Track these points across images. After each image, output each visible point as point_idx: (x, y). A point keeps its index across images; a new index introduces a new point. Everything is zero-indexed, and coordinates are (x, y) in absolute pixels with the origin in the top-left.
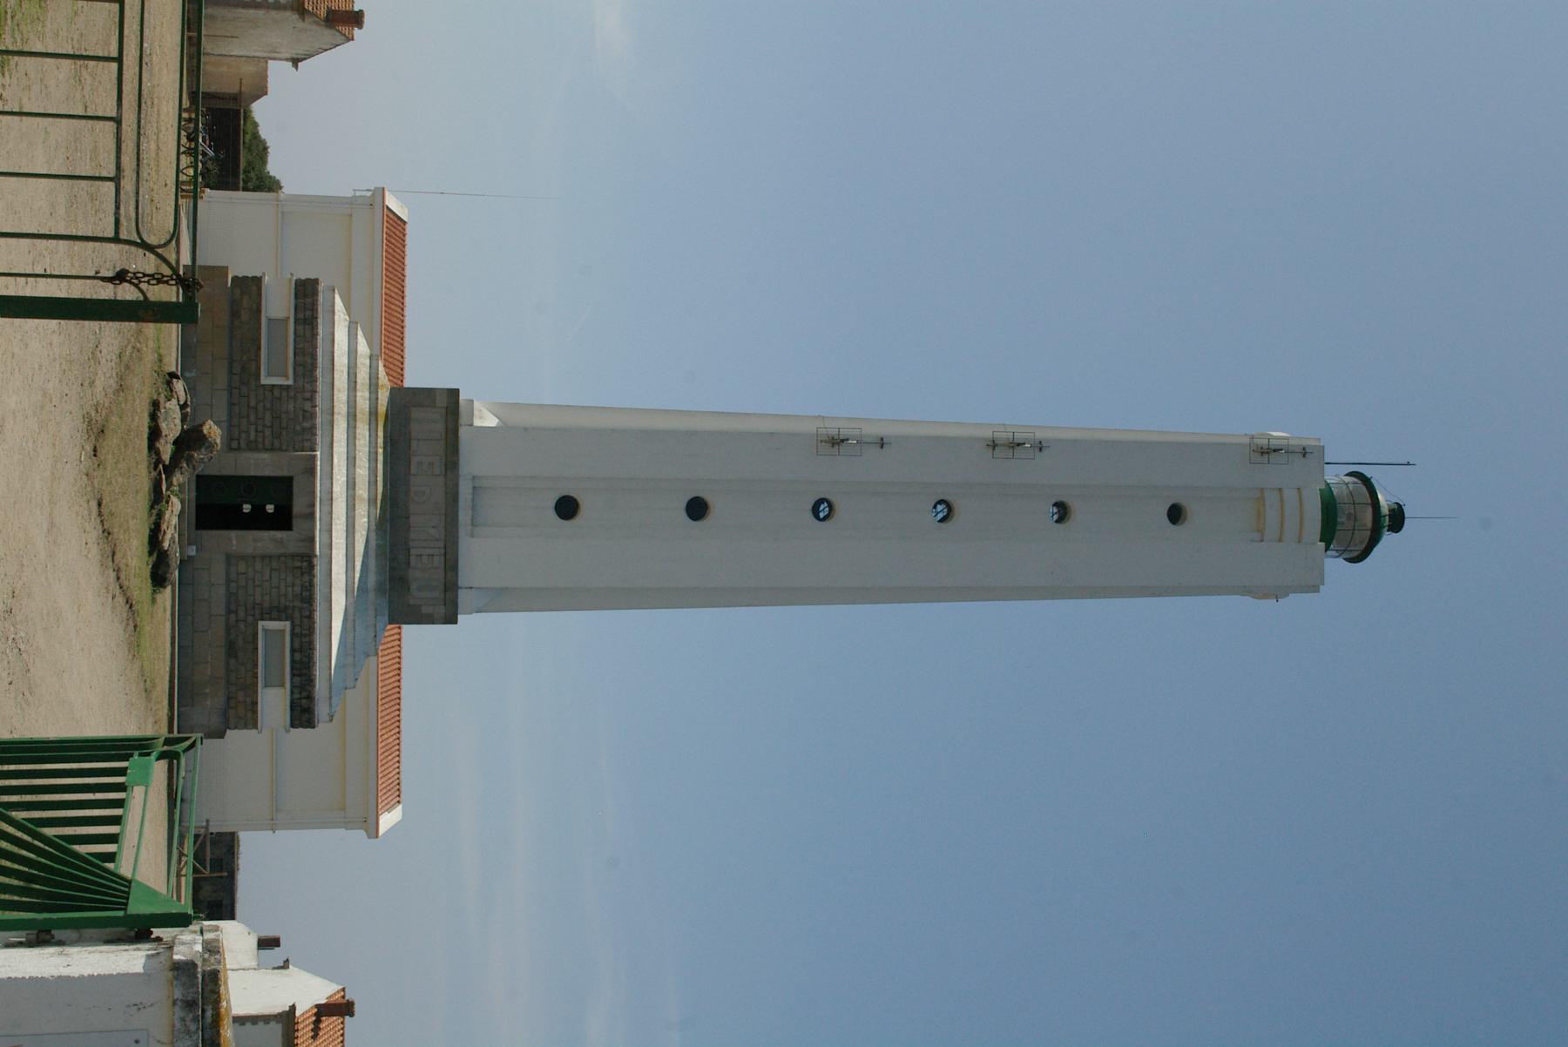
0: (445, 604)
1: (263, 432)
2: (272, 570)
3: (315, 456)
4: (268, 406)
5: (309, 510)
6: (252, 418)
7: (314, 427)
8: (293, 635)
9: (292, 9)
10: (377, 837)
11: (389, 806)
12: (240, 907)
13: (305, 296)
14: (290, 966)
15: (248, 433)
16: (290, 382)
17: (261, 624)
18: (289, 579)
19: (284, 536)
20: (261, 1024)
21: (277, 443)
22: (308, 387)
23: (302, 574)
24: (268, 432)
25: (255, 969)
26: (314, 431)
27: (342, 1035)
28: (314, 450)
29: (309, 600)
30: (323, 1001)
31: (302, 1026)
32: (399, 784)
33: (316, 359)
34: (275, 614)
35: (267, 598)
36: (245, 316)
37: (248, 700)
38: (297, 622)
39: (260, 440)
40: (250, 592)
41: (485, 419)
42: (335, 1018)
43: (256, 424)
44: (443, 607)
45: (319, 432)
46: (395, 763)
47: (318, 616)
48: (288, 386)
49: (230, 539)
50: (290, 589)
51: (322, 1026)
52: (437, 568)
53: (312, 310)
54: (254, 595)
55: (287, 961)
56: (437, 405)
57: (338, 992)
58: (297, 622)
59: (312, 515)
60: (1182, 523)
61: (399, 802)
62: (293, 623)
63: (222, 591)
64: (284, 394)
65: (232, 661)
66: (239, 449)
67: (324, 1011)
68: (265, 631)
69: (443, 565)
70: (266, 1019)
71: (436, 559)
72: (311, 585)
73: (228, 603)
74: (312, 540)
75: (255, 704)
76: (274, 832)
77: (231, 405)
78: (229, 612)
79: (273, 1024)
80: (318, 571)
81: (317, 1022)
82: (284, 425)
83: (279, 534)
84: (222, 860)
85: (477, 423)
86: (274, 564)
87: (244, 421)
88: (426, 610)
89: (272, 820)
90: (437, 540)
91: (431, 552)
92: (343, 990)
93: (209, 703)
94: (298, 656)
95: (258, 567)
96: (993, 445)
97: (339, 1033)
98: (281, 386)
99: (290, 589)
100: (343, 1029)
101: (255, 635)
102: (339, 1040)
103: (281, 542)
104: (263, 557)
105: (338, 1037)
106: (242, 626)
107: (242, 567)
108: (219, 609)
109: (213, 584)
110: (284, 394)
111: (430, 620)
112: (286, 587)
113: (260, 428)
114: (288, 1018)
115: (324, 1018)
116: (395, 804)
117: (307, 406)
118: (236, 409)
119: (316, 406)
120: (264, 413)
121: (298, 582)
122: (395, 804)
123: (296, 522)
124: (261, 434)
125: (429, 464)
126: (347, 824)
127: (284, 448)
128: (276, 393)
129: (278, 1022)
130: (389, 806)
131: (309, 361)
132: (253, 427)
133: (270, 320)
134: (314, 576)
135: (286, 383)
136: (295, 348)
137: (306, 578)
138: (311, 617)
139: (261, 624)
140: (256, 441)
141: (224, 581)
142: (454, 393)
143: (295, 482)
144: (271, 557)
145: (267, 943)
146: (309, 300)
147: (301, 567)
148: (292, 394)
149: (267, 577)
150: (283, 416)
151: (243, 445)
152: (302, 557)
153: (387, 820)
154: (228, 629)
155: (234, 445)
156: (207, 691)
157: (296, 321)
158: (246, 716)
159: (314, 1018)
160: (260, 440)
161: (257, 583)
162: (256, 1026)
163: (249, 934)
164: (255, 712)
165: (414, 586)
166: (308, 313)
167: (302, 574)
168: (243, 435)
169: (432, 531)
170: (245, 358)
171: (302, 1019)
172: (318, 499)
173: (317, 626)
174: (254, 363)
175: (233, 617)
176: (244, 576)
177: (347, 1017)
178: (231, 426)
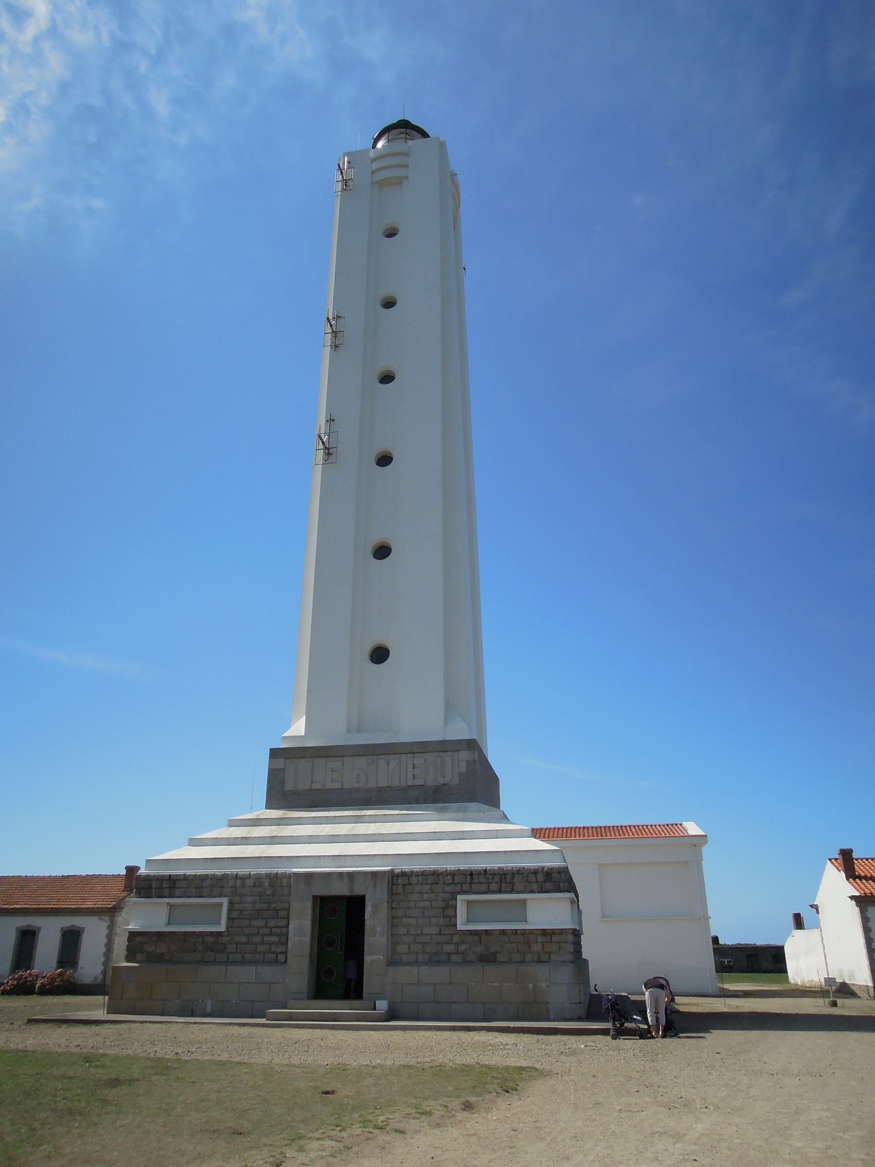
0: (458, 751)
1: (271, 928)
2: (406, 916)
4: (246, 922)
5: (346, 880)
6: (257, 939)
7: (268, 875)
9: (113, 916)
10: (706, 836)
11: (683, 830)
12: (774, 942)
13: (150, 888)
14: (815, 903)
15: (271, 944)
16: (225, 901)
17: (460, 927)
18: (415, 897)
19: (370, 904)
20: (870, 925)
21: (283, 913)
22: (231, 883)
23: (410, 884)
24: (272, 923)
26: (272, 875)
27: (867, 859)
30: (843, 874)
31: (866, 890)
32: (668, 825)
34: (450, 912)
36: (162, 949)
37: (540, 939)
38: (458, 888)
39: (278, 931)
40: (428, 938)
41: (298, 728)
42: (856, 867)
43: (263, 935)
44: (460, 752)
45: (275, 870)
46: (656, 828)
47: (451, 867)
49: (372, 962)
50: (426, 896)
51: (862, 874)
52: (425, 760)
53: (163, 880)
54: (431, 935)
56: (283, 767)
57: (833, 863)
58: (458, 888)
59: (351, 875)
61: (681, 825)
62: (459, 893)
63: (425, 970)
65: (500, 958)
66: (285, 953)
67: (851, 874)
68: (469, 921)
69: (422, 755)
70: (865, 921)
71: (416, 761)
72: (423, 874)
73: (438, 962)
74: (374, 874)
75: (544, 932)
76: (710, 917)
77: (243, 962)
78: (448, 961)
79: (868, 914)
80: (406, 868)
81: (860, 877)
83: (368, 910)
84: (747, 955)
87: (260, 948)
89: (701, 919)
90: (400, 761)
91: (410, 767)
92: (830, 860)
93: (544, 985)
94: (494, 886)
95: (402, 931)
96: (335, 347)
97: (866, 862)
98: (229, 910)
100: (862, 859)
101: (471, 933)
102: (872, 862)
103: (375, 907)
105: (870, 863)
106: (463, 947)
107: (403, 948)
108: (441, 973)
109: (418, 981)
110: (237, 906)
112: (423, 900)
113: (267, 931)
114: (862, 901)
115: (857, 873)
116: (682, 827)
117: (250, 882)
118: (248, 956)
119: (237, 875)
120: (253, 927)
121: (418, 888)
122: (682, 827)
123: (358, 891)
124: (273, 930)
126: (699, 859)
127: (287, 905)
128: (235, 915)
130: (683, 830)
131: (208, 882)
132: (266, 939)
133: (169, 923)
134: (412, 872)
136: (195, 897)
137: (414, 880)
138: (454, 874)
139: (460, 927)
140: (280, 935)
141: (415, 968)
142: (275, 753)
145: (798, 922)
148: (237, 899)
149: (413, 921)
150: (257, 907)
151: (283, 949)
152: (393, 884)
153: (693, 829)
154: (466, 962)
155: (281, 958)
156: (531, 986)
157: (171, 896)
158: (557, 943)
159: (864, 881)
160: (278, 931)
161: (420, 932)
162: (872, 928)
163: (793, 936)
164: (553, 932)
167: (410, 884)
168: (273, 948)
169: (391, 767)
170: (201, 948)
171: (861, 890)
172: (337, 869)
173: (462, 867)
174: (207, 939)
175: (454, 958)
176: (411, 946)
177: (854, 855)
178: (264, 962)
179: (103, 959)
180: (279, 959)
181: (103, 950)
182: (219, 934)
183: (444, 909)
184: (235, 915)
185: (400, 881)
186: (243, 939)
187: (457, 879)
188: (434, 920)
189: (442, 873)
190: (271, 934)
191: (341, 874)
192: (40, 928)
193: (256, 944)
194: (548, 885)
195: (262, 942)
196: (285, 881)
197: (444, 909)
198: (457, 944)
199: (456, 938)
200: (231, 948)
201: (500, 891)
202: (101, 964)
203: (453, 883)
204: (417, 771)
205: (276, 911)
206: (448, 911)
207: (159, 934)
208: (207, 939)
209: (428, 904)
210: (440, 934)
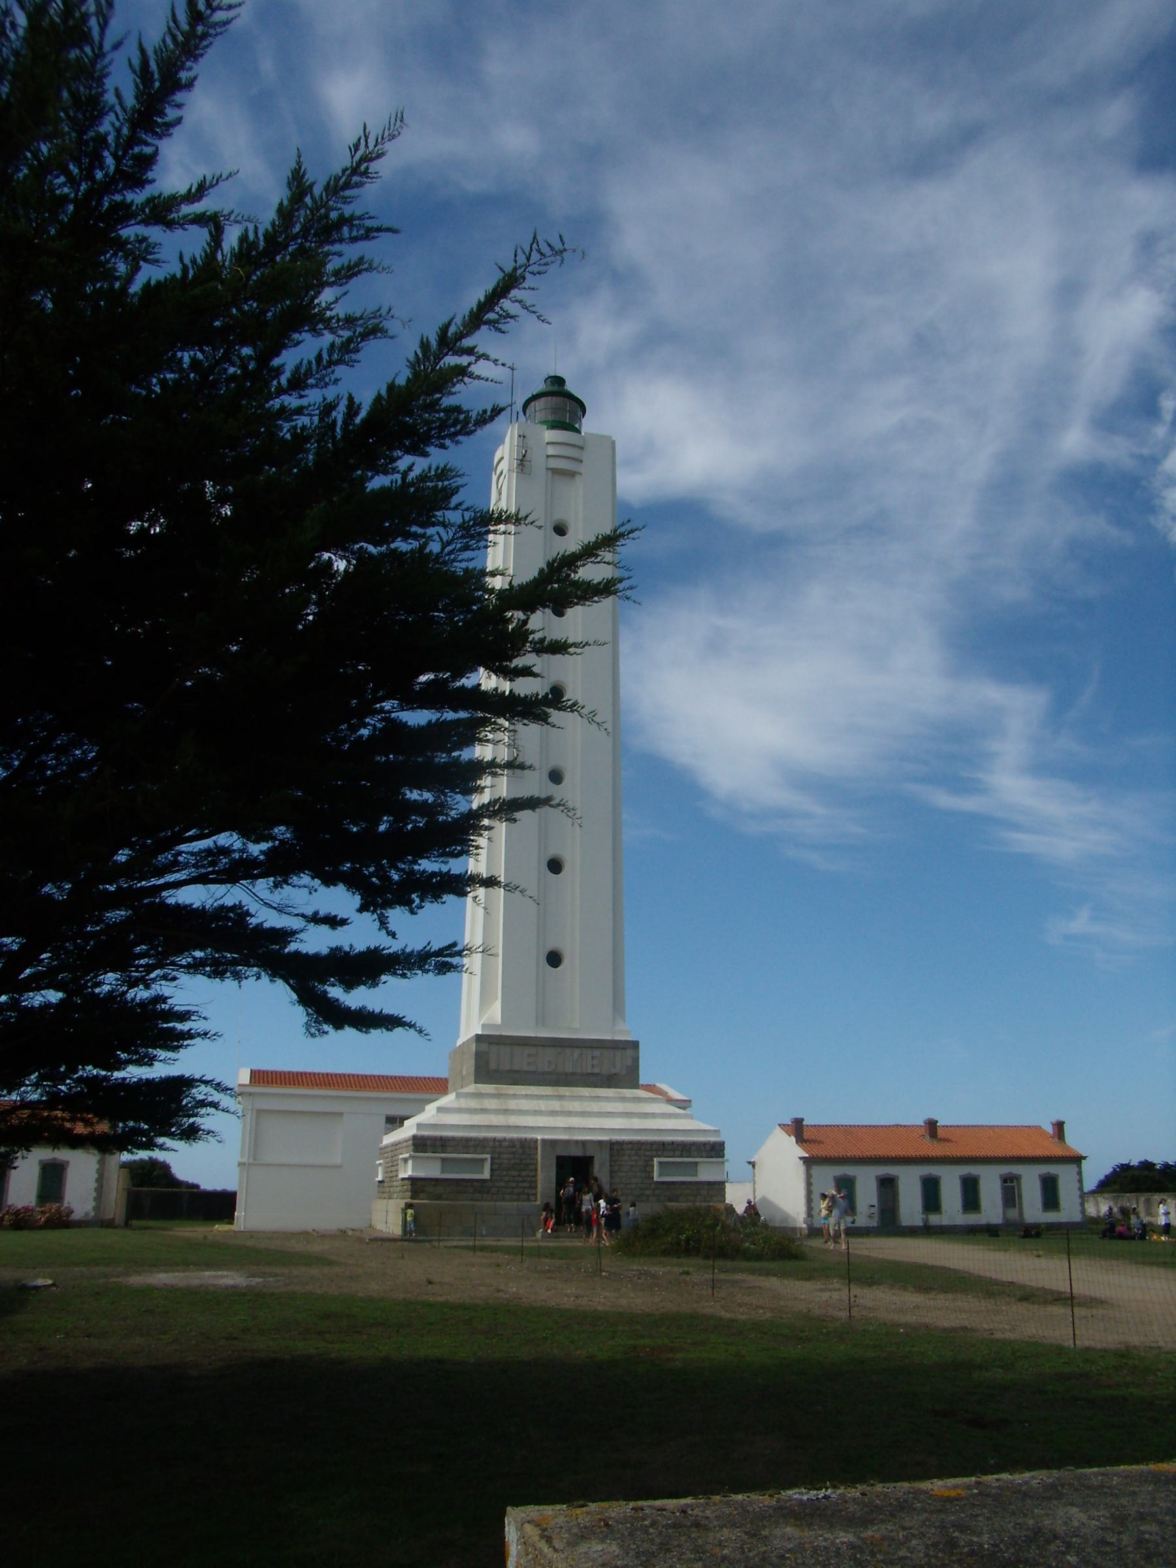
0: (626, 1049)
3: (543, 1141)
4: (505, 1173)
6: (513, 1185)
8: (659, 1156)
10: (690, 1101)
16: (488, 1156)
17: (655, 1180)
18: (626, 1158)
22: (491, 1144)
25: (754, 1184)
28: (536, 1140)
29: (640, 1144)
30: (793, 1139)
33: (472, 1138)
35: (639, 1174)
37: (706, 1187)
43: (518, 1182)
48: (492, 1158)
55: (749, 1163)
58: (654, 1153)
60: (567, 528)
64: (496, 1161)
67: (801, 1139)
74: (600, 1142)
79: (812, 1172)
82: (518, 1161)
85: (499, 1021)
86: (616, 1168)
87: (516, 1191)
88: (629, 1063)
94: (678, 1153)
99: (633, 1158)
104: (611, 1177)
106: (657, 1192)
111: (636, 1060)
113: (521, 1179)
121: (628, 1152)
125: (593, 1059)
129: (811, 1168)
135: (489, 1161)
140: (530, 1182)
143: (560, 1154)
144: (611, 1172)
146: (429, 1142)
147: (618, 1150)
148: (497, 1156)
165: (614, 1071)
166: (438, 1143)
167: (622, 1149)
177: (804, 1123)
179: (94, 1194)
180: (530, 1196)
181: (93, 1185)
182: (484, 1181)
183: (645, 1167)
184: (495, 1167)
185: (615, 1148)
186: (503, 1184)
187: (654, 1147)
188: (639, 1174)
189: (644, 1143)
190: (523, 1181)
191: (577, 1142)
192: (68, 1162)
193: (513, 1188)
194: (713, 1153)
195: (517, 1187)
196: (532, 1143)
197: (645, 1167)
198: (653, 1190)
199: (653, 1186)
200: (494, 1190)
201: (681, 1156)
202: (92, 1200)
203: (652, 1150)
204: (595, 1062)
205: (527, 1165)
206: (647, 1168)
207: (436, 1180)
208: (475, 1184)
209: (634, 1163)
210: (642, 1183)
